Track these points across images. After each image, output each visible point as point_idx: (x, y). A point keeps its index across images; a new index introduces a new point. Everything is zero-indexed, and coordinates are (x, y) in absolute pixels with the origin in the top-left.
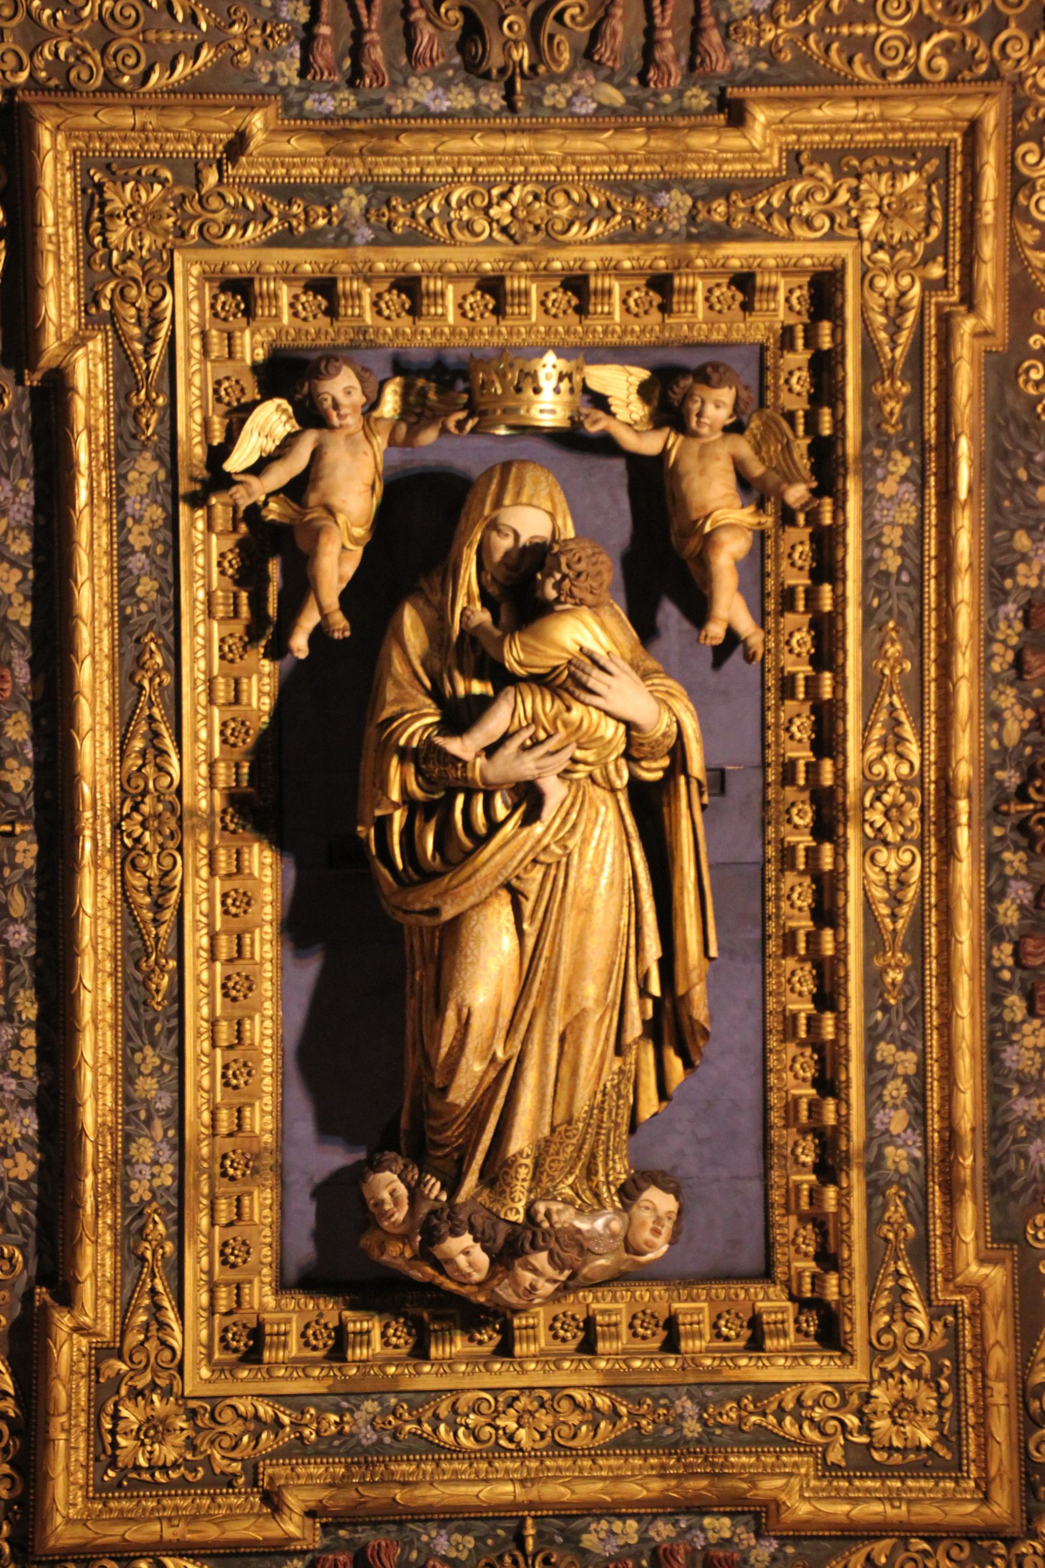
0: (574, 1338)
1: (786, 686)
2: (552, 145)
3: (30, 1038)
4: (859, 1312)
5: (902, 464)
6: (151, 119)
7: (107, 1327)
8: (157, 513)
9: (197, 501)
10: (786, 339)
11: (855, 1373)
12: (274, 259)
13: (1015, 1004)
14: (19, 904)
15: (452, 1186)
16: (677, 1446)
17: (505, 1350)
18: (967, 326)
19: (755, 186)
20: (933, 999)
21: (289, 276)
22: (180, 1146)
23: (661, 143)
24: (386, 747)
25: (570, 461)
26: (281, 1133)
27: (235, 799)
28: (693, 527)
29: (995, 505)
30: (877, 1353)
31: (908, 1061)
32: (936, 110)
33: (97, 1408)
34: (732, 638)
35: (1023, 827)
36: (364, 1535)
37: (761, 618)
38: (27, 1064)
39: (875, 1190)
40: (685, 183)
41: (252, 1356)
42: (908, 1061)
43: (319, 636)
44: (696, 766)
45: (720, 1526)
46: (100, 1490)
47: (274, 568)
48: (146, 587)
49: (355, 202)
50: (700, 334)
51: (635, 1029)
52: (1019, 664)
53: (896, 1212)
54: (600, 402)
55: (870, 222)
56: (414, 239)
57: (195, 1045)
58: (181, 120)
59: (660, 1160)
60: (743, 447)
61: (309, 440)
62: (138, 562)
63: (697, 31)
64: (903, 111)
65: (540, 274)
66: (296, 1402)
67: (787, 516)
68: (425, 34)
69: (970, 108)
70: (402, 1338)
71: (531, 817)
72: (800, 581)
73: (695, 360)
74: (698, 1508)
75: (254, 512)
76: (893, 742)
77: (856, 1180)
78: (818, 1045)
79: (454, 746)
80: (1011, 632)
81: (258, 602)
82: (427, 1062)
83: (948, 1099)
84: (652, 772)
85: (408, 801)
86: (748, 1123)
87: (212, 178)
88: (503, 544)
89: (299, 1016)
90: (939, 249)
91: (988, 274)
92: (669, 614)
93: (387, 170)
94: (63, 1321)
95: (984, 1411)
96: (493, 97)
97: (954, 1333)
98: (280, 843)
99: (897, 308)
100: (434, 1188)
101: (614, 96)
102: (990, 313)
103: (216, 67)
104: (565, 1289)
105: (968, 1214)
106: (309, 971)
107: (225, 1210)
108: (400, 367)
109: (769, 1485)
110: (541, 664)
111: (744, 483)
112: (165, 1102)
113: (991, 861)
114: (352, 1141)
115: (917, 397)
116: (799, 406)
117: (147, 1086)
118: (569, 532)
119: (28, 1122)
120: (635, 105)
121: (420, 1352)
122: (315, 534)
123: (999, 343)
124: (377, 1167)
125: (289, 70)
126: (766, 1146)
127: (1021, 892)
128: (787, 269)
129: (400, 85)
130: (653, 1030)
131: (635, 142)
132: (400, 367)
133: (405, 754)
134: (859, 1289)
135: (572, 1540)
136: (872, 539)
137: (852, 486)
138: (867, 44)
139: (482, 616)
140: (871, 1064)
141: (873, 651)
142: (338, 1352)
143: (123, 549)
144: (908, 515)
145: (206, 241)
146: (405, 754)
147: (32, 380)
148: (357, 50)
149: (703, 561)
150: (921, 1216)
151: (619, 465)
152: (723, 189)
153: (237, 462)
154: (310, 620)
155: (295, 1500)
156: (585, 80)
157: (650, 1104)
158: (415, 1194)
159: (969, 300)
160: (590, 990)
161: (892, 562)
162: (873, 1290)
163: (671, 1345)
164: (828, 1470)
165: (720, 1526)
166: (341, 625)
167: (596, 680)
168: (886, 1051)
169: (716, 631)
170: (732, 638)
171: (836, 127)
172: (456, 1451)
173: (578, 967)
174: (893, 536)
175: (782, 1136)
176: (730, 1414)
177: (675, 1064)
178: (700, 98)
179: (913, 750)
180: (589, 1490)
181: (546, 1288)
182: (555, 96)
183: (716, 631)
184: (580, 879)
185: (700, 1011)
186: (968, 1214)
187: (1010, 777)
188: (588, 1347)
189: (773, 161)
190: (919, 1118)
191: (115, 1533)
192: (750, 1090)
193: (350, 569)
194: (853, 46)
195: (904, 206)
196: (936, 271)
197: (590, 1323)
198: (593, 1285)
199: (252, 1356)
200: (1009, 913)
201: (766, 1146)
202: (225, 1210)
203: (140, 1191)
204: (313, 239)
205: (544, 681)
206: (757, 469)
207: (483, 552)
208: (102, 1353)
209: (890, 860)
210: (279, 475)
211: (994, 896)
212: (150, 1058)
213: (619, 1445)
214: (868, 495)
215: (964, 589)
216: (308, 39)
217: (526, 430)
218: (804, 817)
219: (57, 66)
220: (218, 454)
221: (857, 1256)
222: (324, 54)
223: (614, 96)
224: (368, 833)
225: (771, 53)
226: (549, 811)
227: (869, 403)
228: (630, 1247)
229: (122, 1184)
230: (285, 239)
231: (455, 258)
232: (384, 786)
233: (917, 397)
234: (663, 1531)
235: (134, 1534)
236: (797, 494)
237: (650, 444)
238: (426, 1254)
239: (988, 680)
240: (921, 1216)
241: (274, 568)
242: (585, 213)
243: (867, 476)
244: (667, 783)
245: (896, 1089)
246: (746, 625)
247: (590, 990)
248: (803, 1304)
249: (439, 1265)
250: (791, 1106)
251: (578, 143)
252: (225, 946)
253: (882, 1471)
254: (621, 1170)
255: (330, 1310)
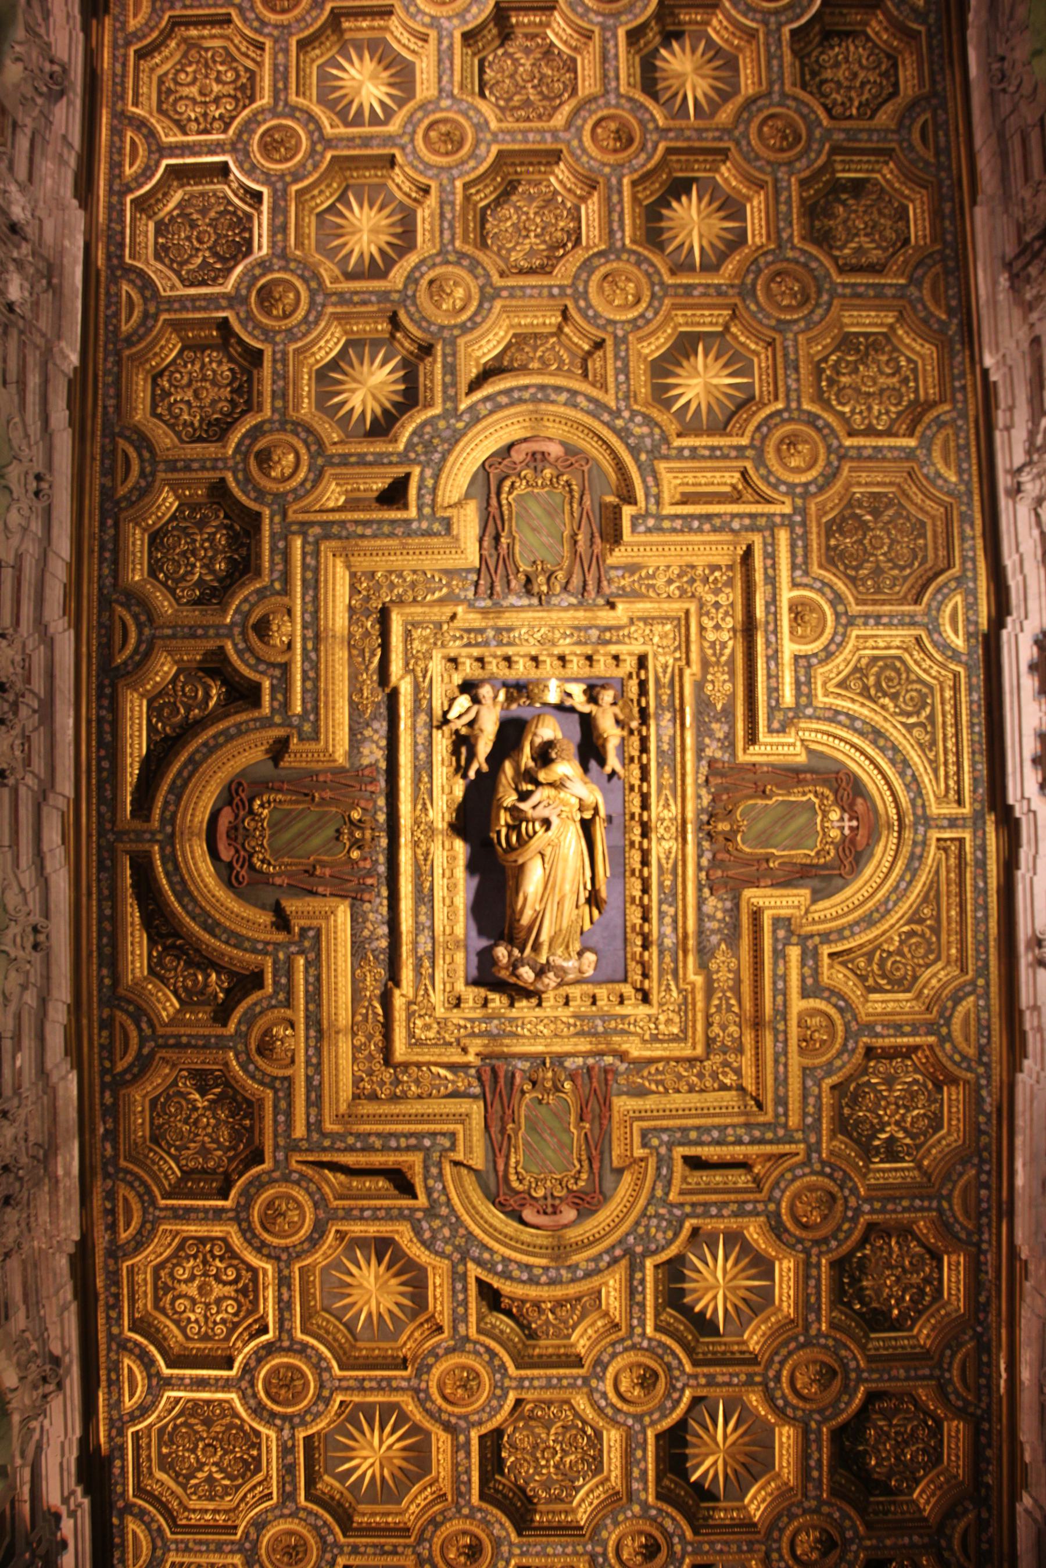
0: (562, 1001)
1: (632, 788)
2: (554, 615)
3: (385, 902)
4: (655, 991)
5: (668, 716)
6: (426, 609)
7: (411, 995)
8: (426, 732)
9: (439, 728)
10: (630, 676)
11: (653, 1011)
12: (465, 651)
13: (706, 892)
14: (382, 859)
15: (522, 951)
16: (596, 1034)
17: (539, 1005)
18: (687, 672)
19: (619, 628)
20: (680, 890)
21: (469, 657)
22: (433, 938)
23: (589, 614)
24: (500, 806)
25: (560, 714)
26: (466, 935)
27: (452, 826)
28: (600, 736)
29: (698, 729)
30: (661, 1005)
31: (671, 911)
32: (676, 606)
33: (408, 1020)
34: (614, 773)
35: (709, 834)
36: (494, 1062)
37: (623, 765)
38: (384, 910)
39: (661, 952)
40: (597, 627)
41: (457, 1006)
42: (671, 911)
43: (478, 772)
44: (602, 812)
45: (609, 1059)
46: (410, 1045)
47: (464, 750)
48: (422, 756)
49: (491, 633)
50: (603, 674)
51: (582, 900)
52: (707, 781)
53: (668, 959)
54: (569, 695)
55: (656, 640)
56: (509, 644)
57: (438, 905)
58: (436, 610)
59: (591, 943)
60: (616, 710)
61: (475, 708)
62: (420, 748)
63: (599, 581)
64: (665, 606)
65: (551, 655)
66: (472, 1020)
67: (631, 732)
68: (513, 583)
69: (686, 606)
70: (505, 1000)
71: (548, 829)
72: (636, 754)
73: (600, 682)
74: (602, 1054)
75: (457, 732)
76: (667, 805)
77: (654, 950)
78: (642, 905)
79: (522, 806)
80: (704, 770)
81: (458, 761)
82: (513, 911)
83: (685, 923)
84: (588, 815)
85: (507, 825)
86: (619, 932)
87: (445, 627)
88: (538, 741)
89: (471, 897)
90: (679, 647)
91: (694, 656)
92: (593, 764)
93: (501, 623)
94: (397, 993)
95: (694, 1021)
96: (535, 601)
97: (685, 998)
98: (465, 839)
99: (665, 667)
100: (516, 952)
101: (573, 601)
102: (695, 667)
103: (447, 595)
104: (560, 985)
105: (691, 959)
106: (475, 882)
107: (448, 959)
108: (505, 685)
109: (625, 1047)
110: (551, 780)
111: (618, 722)
112: (428, 924)
113: (699, 845)
114: (489, 937)
115: (673, 694)
116: (635, 697)
117: (422, 918)
118: (560, 736)
119: (384, 930)
120: (580, 603)
121: (512, 1005)
122: (476, 738)
123: (698, 677)
124: (496, 945)
125: (470, 595)
126: (625, 939)
127: (708, 855)
128: (630, 654)
129: (505, 598)
130: (588, 901)
131: (581, 614)
132: (505, 685)
133: (506, 809)
134: (655, 984)
135: (561, 1064)
136: (659, 740)
137: (652, 723)
138: (653, 586)
139: (531, 764)
140: (660, 912)
141: (660, 776)
142: (485, 1005)
143: (415, 744)
144: (671, 732)
145: (443, 646)
146: (506, 809)
147: (388, 690)
148: (492, 588)
149: (604, 746)
150: (675, 961)
151: (576, 716)
152: (609, 629)
153: (451, 716)
154: (474, 767)
155: (472, 1050)
156: (564, 596)
157: (587, 926)
158: (510, 954)
159: (688, 663)
160: (567, 887)
161: (666, 747)
162: (660, 984)
163: (594, 1003)
164: (644, 1041)
165: (609, 1059)
166: (485, 768)
167: (568, 784)
168: (665, 907)
169: (608, 769)
170: (614, 773)
171: (645, 610)
172: (523, 1036)
173: (563, 880)
174: (666, 739)
175: (630, 936)
176: (613, 1024)
177: (596, 912)
178: (601, 601)
179: (673, 808)
180: (568, 1048)
181: (553, 984)
182: (555, 601)
183: (608, 769)
184: (563, 850)
185: (604, 894)
186: (691, 959)
187: (704, 817)
188: (567, 1004)
189: (625, 621)
190: (675, 929)
191: (415, 1058)
192: (620, 921)
193: (488, 749)
194: (649, 587)
195: (666, 635)
196: (677, 655)
197: (567, 997)
198: (568, 984)
199: (457, 1006)
200: (704, 862)
201: (625, 939)
202: (448, 959)
203: (421, 952)
204: (477, 645)
205: (551, 785)
206: (621, 717)
207: (532, 743)
208: (410, 1003)
209: (666, 845)
210: (466, 719)
211: (700, 856)
212: (423, 909)
213: (577, 1034)
214: (658, 725)
215: (689, 756)
216: (477, 584)
217: (545, 704)
218: (638, 830)
219: (399, 596)
220: (445, 713)
221: (654, 973)
222: (481, 589)
223: (573, 601)
224: (494, 836)
225: (623, 588)
226: (554, 827)
227: (658, 696)
228: (581, 971)
229: (415, 950)
230: (469, 645)
231: (522, 650)
232: (498, 819)
233: (673, 694)
234: (591, 1061)
235: (421, 1059)
236: (634, 724)
237: (586, 708)
238: (514, 973)
239: (698, 786)
240: (675, 961)
241: (464, 750)
242: (564, 636)
243: (657, 717)
244: (592, 820)
245: (668, 920)
246: (618, 768)
247: (567, 887)
248: (637, 990)
249: (518, 977)
250: (634, 926)
251: (563, 615)
252: (448, 873)
253: (662, 1041)
254: (577, 946)
255: (482, 992)
